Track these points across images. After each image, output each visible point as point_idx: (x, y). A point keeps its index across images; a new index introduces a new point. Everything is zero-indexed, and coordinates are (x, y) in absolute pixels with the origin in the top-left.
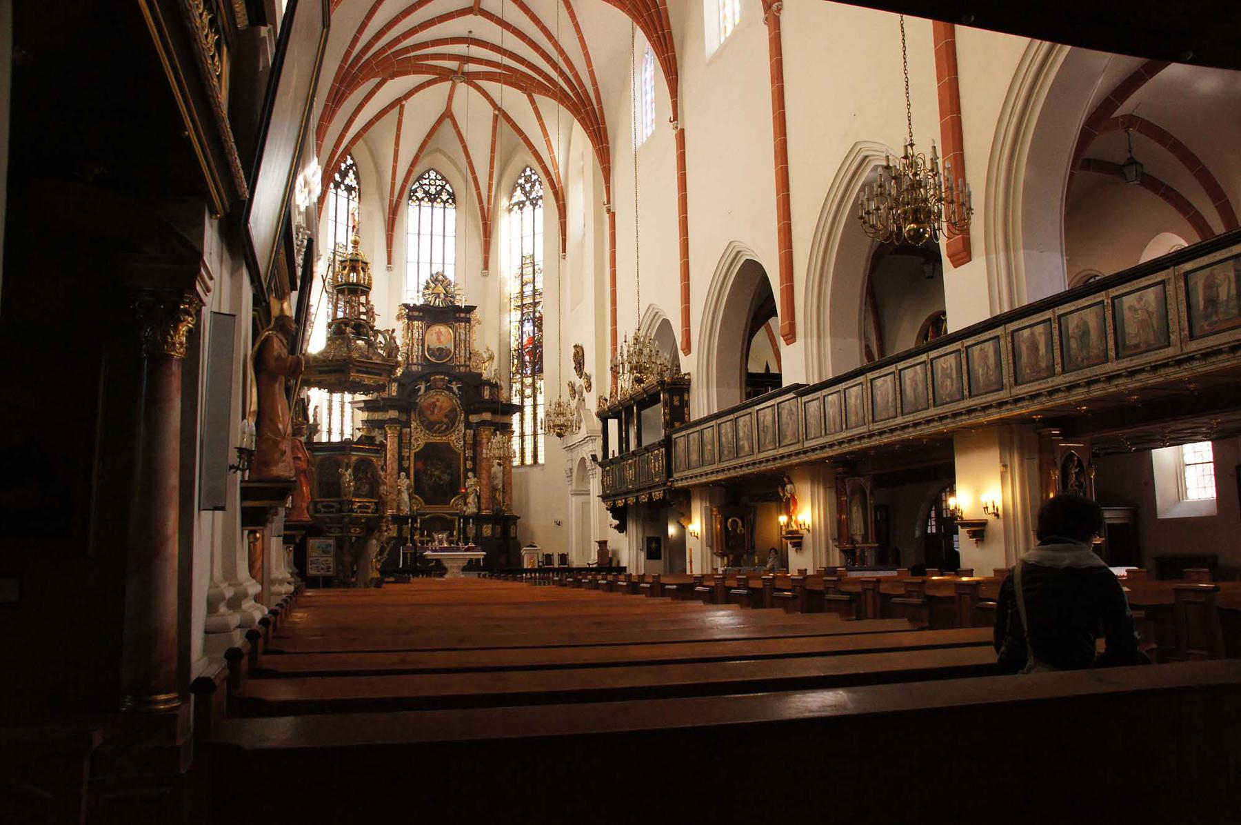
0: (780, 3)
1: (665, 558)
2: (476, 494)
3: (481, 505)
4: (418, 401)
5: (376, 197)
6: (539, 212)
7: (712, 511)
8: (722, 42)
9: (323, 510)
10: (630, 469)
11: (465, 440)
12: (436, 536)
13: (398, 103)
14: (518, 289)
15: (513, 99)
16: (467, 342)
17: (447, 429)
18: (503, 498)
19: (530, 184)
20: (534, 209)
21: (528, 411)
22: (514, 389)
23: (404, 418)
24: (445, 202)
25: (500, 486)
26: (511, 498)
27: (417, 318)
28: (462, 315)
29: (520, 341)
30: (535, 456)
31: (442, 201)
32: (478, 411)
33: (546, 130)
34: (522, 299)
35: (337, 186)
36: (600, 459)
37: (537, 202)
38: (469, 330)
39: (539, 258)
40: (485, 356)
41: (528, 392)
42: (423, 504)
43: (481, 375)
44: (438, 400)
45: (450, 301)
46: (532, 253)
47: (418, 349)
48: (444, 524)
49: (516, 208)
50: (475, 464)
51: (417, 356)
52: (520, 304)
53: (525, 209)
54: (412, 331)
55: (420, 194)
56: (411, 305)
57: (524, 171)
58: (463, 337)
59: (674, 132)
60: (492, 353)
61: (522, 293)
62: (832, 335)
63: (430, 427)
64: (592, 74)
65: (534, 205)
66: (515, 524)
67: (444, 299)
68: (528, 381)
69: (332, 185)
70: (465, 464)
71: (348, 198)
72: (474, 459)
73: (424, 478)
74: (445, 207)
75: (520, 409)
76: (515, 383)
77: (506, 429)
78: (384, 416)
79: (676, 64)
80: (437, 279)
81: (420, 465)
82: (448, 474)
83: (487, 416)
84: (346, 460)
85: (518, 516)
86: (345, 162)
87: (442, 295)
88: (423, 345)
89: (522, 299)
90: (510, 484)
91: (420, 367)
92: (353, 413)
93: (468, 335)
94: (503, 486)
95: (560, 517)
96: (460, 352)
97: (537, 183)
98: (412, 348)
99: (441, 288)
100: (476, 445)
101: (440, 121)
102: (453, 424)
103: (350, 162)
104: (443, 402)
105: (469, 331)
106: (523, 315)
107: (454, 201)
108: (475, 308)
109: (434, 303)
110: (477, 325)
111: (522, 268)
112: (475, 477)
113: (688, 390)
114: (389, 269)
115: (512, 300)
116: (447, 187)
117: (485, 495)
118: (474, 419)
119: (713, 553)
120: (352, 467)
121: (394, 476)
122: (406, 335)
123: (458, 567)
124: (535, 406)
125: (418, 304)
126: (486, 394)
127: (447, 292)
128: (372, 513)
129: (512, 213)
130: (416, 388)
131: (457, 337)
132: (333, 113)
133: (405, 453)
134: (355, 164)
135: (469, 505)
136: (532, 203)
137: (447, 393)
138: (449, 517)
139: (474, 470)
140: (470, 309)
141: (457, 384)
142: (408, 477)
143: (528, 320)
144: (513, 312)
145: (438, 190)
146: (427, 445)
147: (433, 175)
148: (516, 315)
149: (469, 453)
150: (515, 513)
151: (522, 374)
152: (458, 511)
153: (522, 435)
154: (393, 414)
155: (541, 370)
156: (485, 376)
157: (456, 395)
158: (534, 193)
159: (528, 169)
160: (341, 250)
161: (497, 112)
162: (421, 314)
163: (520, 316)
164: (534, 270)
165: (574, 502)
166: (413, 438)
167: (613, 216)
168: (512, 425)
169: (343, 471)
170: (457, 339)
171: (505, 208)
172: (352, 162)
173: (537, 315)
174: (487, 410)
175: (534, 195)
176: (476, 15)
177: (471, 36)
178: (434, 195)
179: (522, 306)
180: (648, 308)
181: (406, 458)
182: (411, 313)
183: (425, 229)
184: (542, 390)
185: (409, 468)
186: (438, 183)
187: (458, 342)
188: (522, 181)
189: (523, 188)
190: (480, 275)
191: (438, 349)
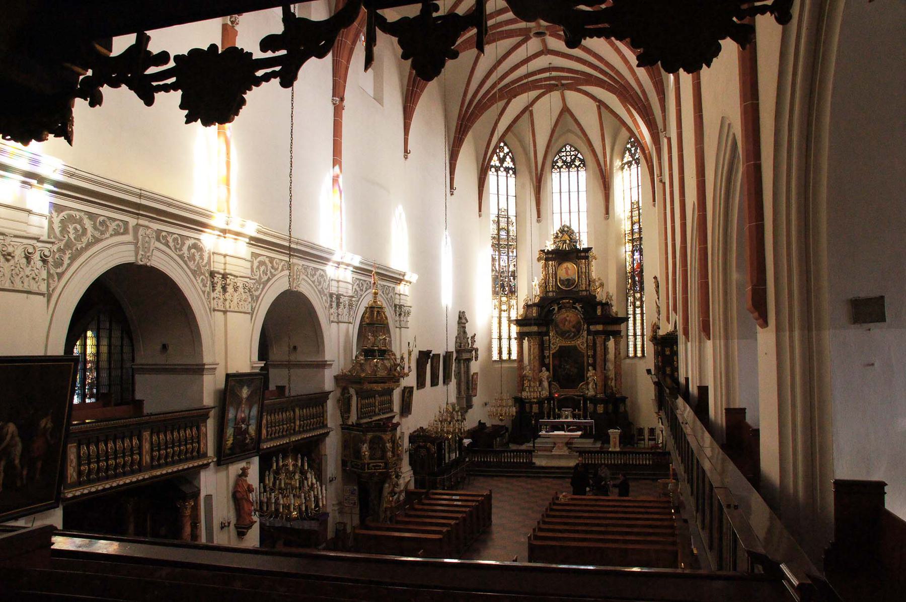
5: (527, 173)
13: (527, 109)
17: (574, 336)
22: (629, 301)
23: (544, 329)
27: (552, 259)
28: (583, 254)
34: (632, 235)
35: (497, 169)
38: (588, 265)
41: (638, 303)
44: (568, 316)
45: (574, 245)
46: (637, 200)
49: (626, 166)
51: (552, 286)
53: (632, 167)
55: (560, 164)
58: (584, 270)
61: (632, 230)
63: (563, 334)
71: (507, 177)
74: (578, 171)
76: (630, 296)
77: (617, 334)
81: (556, 362)
83: (600, 327)
86: (503, 151)
87: (568, 242)
89: (632, 235)
90: (620, 373)
99: (566, 237)
102: (579, 332)
103: (506, 150)
104: (571, 317)
114: (538, 221)
117: (600, 384)
118: (592, 328)
120: (368, 442)
123: (562, 443)
124: (642, 314)
126: (599, 312)
128: (383, 469)
129: (624, 170)
133: (546, 353)
134: (510, 151)
136: (636, 163)
137: (574, 310)
138: (576, 397)
140: (588, 250)
142: (548, 370)
147: (568, 148)
148: (629, 247)
149: (590, 353)
150: (624, 394)
151: (634, 290)
153: (635, 335)
154: (535, 329)
156: (598, 298)
160: (503, 213)
164: (639, 213)
172: (508, 150)
175: (637, 156)
176: (546, 55)
177: (551, 66)
178: (570, 163)
179: (633, 240)
183: (565, 188)
185: (549, 363)
186: (572, 153)
187: (580, 274)
188: (629, 146)
189: (630, 151)
190: (603, 218)
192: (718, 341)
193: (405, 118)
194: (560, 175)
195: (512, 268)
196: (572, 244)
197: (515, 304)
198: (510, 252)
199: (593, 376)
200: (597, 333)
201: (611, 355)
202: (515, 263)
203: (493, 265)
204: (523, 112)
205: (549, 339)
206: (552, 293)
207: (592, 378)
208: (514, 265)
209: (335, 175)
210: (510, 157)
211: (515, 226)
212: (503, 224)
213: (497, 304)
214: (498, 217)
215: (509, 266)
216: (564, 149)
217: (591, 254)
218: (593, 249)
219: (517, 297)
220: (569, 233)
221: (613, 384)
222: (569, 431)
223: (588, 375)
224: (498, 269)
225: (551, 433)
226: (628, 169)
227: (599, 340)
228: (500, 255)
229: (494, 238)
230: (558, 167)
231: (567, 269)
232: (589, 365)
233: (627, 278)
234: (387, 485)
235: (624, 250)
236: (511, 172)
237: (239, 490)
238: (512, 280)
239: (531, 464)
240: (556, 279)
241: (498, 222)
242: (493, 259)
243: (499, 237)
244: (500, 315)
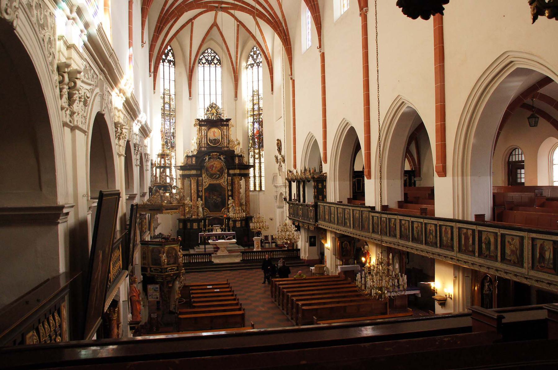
0: (367, 8)
1: (318, 246)
6: (261, 69)
7: (336, 239)
8: (342, 13)
9: (154, 271)
10: (300, 210)
11: (227, 182)
13: (191, 21)
14: (252, 107)
15: (247, 19)
17: (219, 177)
18: (246, 208)
19: (256, 55)
20: (258, 68)
21: (257, 165)
22: (250, 154)
24: (216, 64)
25: (244, 203)
26: (249, 208)
28: (225, 123)
29: (253, 132)
30: (261, 187)
31: (214, 64)
33: (262, 32)
34: (253, 112)
35: (164, 61)
36: (288, 200)
37: (259, 64)
39: (261, 92)
41: (257, 156)
43: (234, 151)
45: (219, 117)
47: (205, 140)
48: (219, 221)
49: (250, 67)
50: (232, 193)
51: (204, 143)
52: (252, 114)
53: (254, 67)
54: (201, 131)
55: (204, 61)
56: (201, 120)
57: (253, 49)
59: (320, 54)
61: (253, 109)
62: (387, 179)
63: (211, 176)
64: (282, 12)
65: (258, 66)
68: (257, 151)
69: (161, 61)
70: (228, 193)
71: (169, 66)
72: (232, 190)
73: (209, 200)
74: (216, 67)
75: (254, 166)
76: (251, 152)
77: (247, 176)
78: (190, 172)
79: (320, 20)
80: (212, 106)
81: (207, 194)
83: (237, 171)
84: (163, 250)
88: (207, 138)
89: (253, 112)
91: (206, 148)
92: (176, 170)
94: (246, 203)
95: (271, 217)
96: (224, 141)
97: (259, 55)
98: (202, 140)
99: (214, 111)
100: (232, 184)
101: (211, 28)
103: (169, 48)
104: (217, 164)
106: (254, 119)
107: (220, 64)
108: (230, 119)
109: (211, 118)
110: (232, 127)
111: (253, 96)
112: (233, 199)
113: (325, 181)
114: (190, 99)
115: (249, 112)
116: (217, 57)
118: (231, 172)
119: (336, 258)
120: (166, 253)
121: (195, 201)
122: (199, 133)
124: (260, 163)
125: (204, 119)
126: (237, 161)
127: (217, 112)
128: (176, 271)
129: (248, 69)
131: (223, 133)
132: (158, 37)
133: (200, 189)
134: (172, 49)
136: (257, 65)
137: (219, 160)
139: (232, 196)
140: (228, 120)
142: (202, 200)
143: (256, 122)
144: (249, 118)
145: (212, 58)
146: (210, 184)
147: (209, 51)
148: (251, 119)
149: (230, 188)
153: (255, 177)
154: (194, 172)
155: (263, 146)
156: (236, 153)
158: (258, 60)
159: (255, 48)
160: (167, 92)
161: (238, 23)
162: (205, 123)
164: (259, 98)
165: (278, 211)
166: (203, 182)
167: (293, 81)
169: (162, 255)
171: (244, 67)
172: (170, 48)
173: (261, 120)
175: (258, 61)
178: (211, 61)
179: (253, 115)
180: (309, 134)
182: (200, 123)
184: (263, 156)
185: (202, 196)
186: (212, 55)
188: (252, 53)
189: (253, 57)
191: (214, 140)
192: (456, 178)
193: (143, 17)
194: (204, 68)
195: (172, 131)
197: (174, 155)
198: (171, 120)
199: (232, 203)
200: (235, 175)
201: (242, 190)
202: (174, 127)
204: (187, 23)
205: (202, 179)
206: (204, 148)
207: (232, 204)
209: (131, 54)
210: (172, 53)
211: (174, 102)
212: (167, 100)
214: (164, 94)
215: (170, 129)
216: (206, 52)
219: (175, 150)
222: (227, 240)
223: (229, 203)
225: (217, 241)
226: (251, 68)
227: (236, 180)
230: (203, 63)
231: (214, 132)
232: (229, 196)
233: (249, 140)
234: (177, 282)
235: (247, 122)
236: (172, 63)
237: (135, 294)
238: (172, 139)
239: (211, 263)
240: (207, 140)
241: (164, 98)
243: (164, 108)
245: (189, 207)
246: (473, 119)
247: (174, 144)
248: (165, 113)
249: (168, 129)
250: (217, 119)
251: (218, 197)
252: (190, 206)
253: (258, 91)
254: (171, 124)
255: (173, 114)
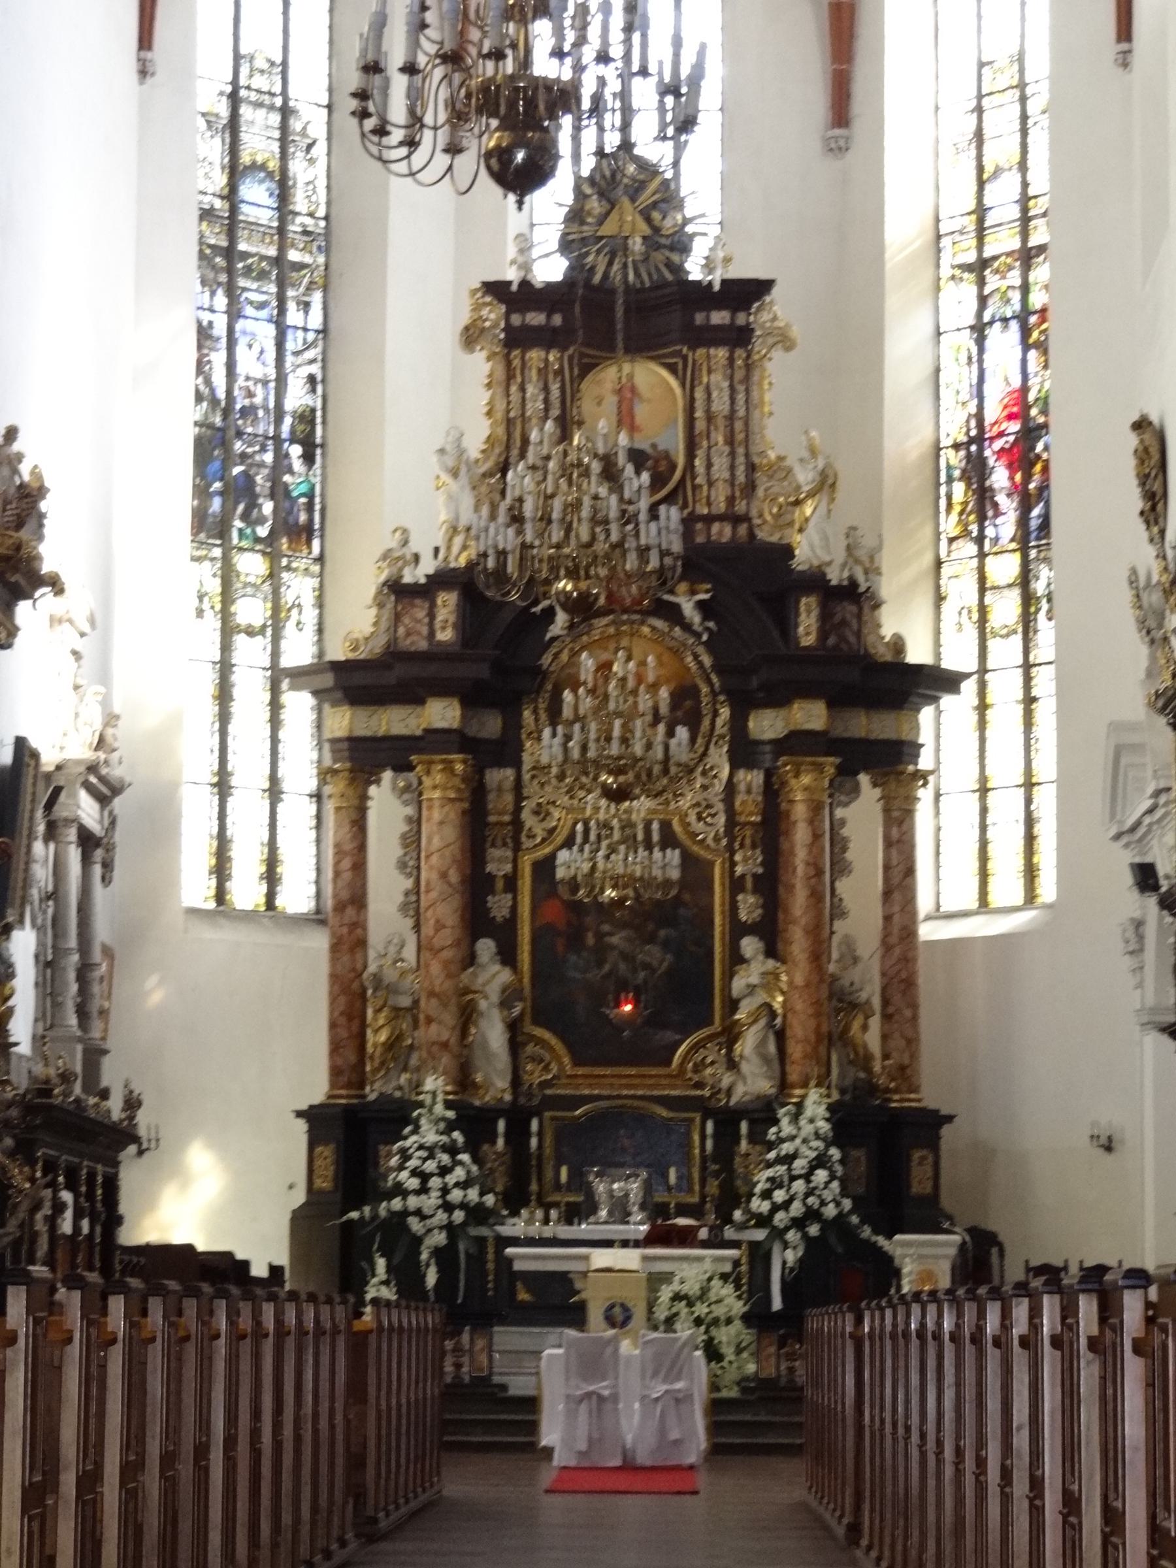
2: (770, 1025)
3: (788, 1068)
4: (546, 660)
12: (600, 1188)
16: (739, 425)
18: (885, 1037)
23: (491, 725)
25: (871, 992)
27: (545, 338)
28: (719, 317)
32: (778, 698)
40: (805, 477)
42: (566, 1060)
43: (787, 551)
45: (669, 265)
46: (1015, 50)
52: (971, 257)
54: (523, 389)
58: (720, 404)
60: (828, 465)
61: (981, 211)
66: (933, 1144)
67: (646, 259)
70: (734, 908)
73: (573, 958)
82: (666, 945)
85: (945, 1111)
93: (741, 397)
95: (1109, 1116)
96: (709, 465)
105: (747, 379)
106: (983, 301)
109: (606, 275)
111: (979, 110)
117: (800, 1030)
130: (537, 609)
133: (498, 863)
135: (745, 1067)
137: (659, 623)
138: (664, 1113)
141: (693, 592)
142: (507, 956)
149: (748, 863)
150: (930, 1097)
151: (980, 540)
152: (707, 1093)
157: (698, 635)
160: (259, 82)
163: (974, 305)
166: (528, 805)
168: (915, 748)
170: (699, 414)
174: (808, 692)
181: (500, 884)
182: (516, 320)
187: (700, 425)
195: (297, 397)
196: (659, 257)
197: (308, 600)
198: (291, 306)
202: (315, 369)
203: (201, 367)
205: (518, 785)
207: (761, 997)
208: (312, 379)
213: (214, 586)
214: (234, 99)
215: (281, 380)
217: (765, 317)
218: (775, 291)
219: (320, 559)
220: (645, 198)
221: (872, 1039)
223: (738, 985)
224: (221, 394)
228: (234, 314)
229: (207, 214)
238: (298, 465)
241: (233, 125)
242: (204, 334)
243: (234, 210)
244: (226, 647)
245: (397, 1011)
246: (867, 1459)
247: (310, 507)
248: (242, 246)
249: (265, 383)
250: (657, 287)
251: (651, 939)
252: (405, 1001)
253: (1020, 59)
254: (290, 346)
255: (307, 259)
